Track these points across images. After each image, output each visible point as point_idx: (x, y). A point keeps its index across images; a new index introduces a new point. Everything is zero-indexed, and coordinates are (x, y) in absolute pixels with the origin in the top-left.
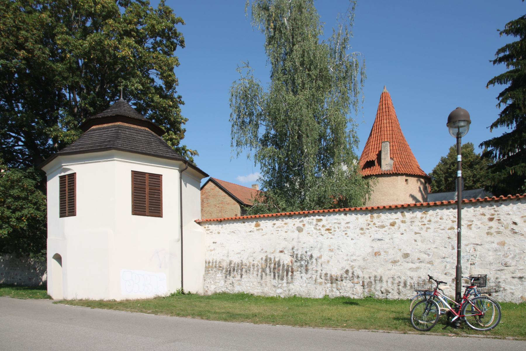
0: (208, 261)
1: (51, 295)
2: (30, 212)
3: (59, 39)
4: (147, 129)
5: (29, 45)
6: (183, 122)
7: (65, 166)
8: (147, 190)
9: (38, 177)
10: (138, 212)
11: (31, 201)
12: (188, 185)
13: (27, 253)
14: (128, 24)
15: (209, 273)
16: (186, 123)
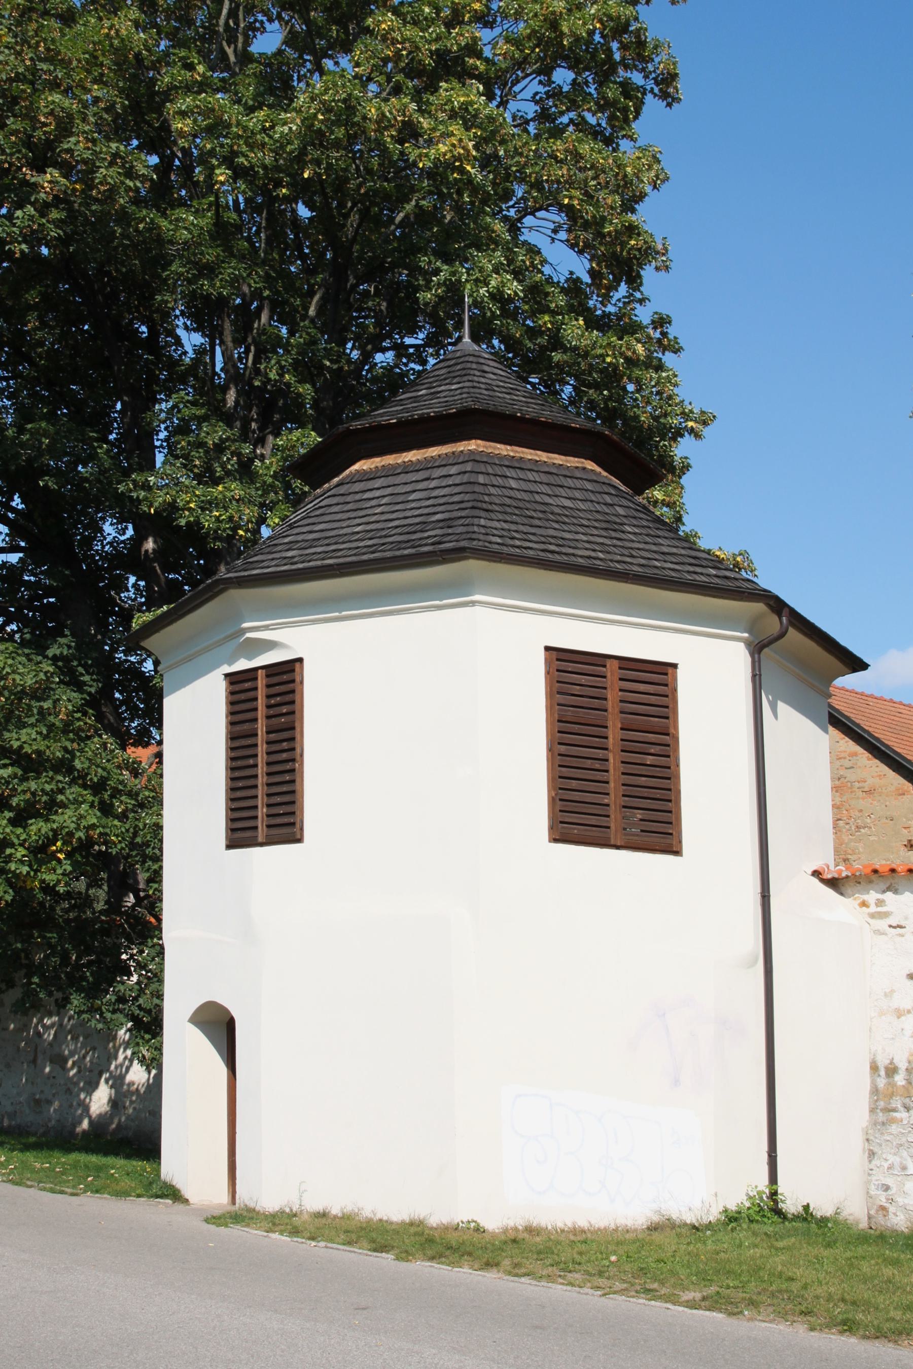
0: (882, 1062)
1: (179, 1182)
2: (84, 823)
3: (183, 114)
4: (590, 465)
5: (77, 145)
6: (692, 431)
7: (256, 629)
8: (614, 735)
9: (87, 678)
10: (576, 830)
11: (83, 775)
12: (782, 706)
13: (58, 995)
14: (449, 25)
15: (893, 1121)
16: (706, 431)
